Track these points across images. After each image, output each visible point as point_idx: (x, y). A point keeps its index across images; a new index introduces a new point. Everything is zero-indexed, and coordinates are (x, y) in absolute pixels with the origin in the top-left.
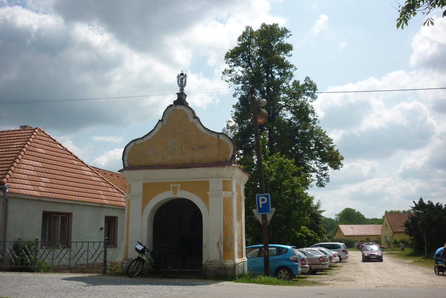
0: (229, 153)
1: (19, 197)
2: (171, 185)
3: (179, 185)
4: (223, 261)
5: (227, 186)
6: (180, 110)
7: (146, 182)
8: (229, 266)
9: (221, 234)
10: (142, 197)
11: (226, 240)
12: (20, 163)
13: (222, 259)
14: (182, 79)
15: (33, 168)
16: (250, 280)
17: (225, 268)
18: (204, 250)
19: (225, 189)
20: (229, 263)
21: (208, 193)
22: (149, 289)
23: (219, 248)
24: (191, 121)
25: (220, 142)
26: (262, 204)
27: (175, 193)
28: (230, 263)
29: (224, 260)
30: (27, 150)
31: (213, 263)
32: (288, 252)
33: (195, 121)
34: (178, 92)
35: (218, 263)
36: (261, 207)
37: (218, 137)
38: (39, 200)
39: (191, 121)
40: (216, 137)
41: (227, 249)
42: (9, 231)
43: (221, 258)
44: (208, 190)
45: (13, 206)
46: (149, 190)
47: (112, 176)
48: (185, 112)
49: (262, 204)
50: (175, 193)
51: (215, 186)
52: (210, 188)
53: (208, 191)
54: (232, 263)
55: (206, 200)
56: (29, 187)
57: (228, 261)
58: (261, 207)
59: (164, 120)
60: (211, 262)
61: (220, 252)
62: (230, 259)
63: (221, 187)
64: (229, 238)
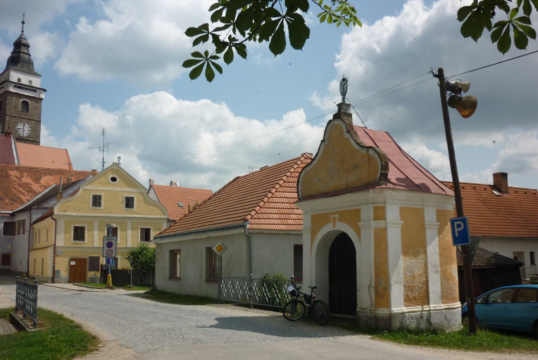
0: (378, 171)
1: (261, 233)
2: (332, 216)
3: (337, 216)
4: (373, 309)
5: (380, 213)
6: (337, 125)
7: (313, 213)
8: (381, 316)
9: (371, 274)
10: (310, 232)
11: (377, 282)
12: (272, 197)
13: (374, 306)
14: (344, 85)
15: (286, 200)
16: (406, 336)
17: (376, 318)
18: (358, 293)
19: (376, 218)
20: (382, 312)
21: (359, 223)
22: (256, 337)
23: (370, 292)
24: (346, 137)
25: (370, 158)
26: (458, 232)
27: (334, 227)
28: (383, 312)
29: (376, 308)
30: (285, 182)
31: (364, 311)
32: (38, 313)
33: (347, 136)
34: (340, 101)
35: (369, 311)
36: (457, 235)
37: (368, 152)
38: (287, 234)
39: (346, 137)
40: (366, 152)
41: (382, 294)
42: (255, 265)
43: (372, 304)
44: (360, 221)
45: (256, 242)
46: (318, 220)
47: (475, 189)
48: (341, 126)
49: (458, 232)
50: (334, 227)
51: (367, 213)
52: (362, 218)
53: (360, 221)
54: (388, 312)
55: (358, 232)
56: (276, 221)
57: (380, 309)
58: (457, 235)
59: (326, 140)
60: (363, 309)
61: (371, 298)
62: (384, 307)
63: (372, 216)
64: (382, 280)
